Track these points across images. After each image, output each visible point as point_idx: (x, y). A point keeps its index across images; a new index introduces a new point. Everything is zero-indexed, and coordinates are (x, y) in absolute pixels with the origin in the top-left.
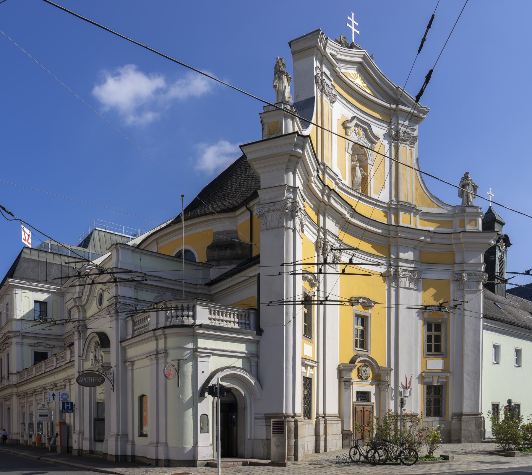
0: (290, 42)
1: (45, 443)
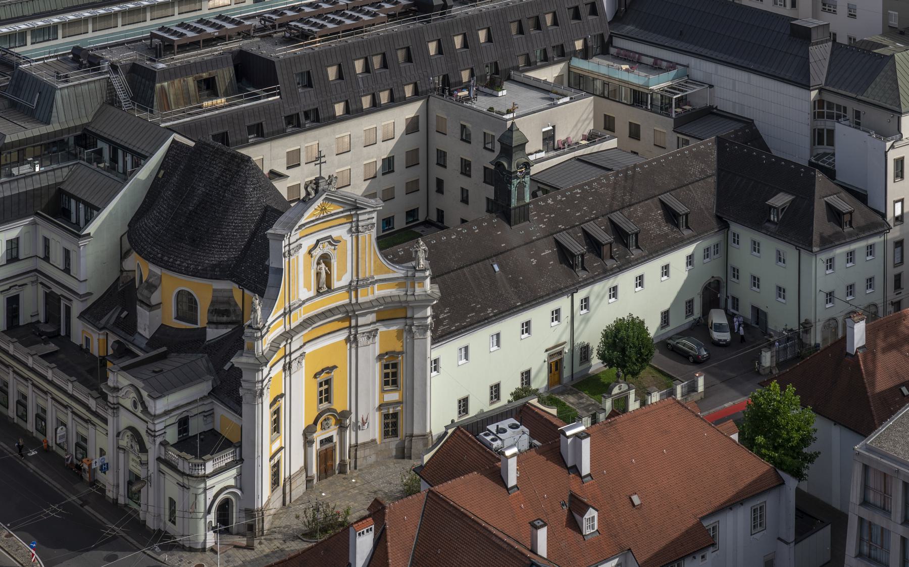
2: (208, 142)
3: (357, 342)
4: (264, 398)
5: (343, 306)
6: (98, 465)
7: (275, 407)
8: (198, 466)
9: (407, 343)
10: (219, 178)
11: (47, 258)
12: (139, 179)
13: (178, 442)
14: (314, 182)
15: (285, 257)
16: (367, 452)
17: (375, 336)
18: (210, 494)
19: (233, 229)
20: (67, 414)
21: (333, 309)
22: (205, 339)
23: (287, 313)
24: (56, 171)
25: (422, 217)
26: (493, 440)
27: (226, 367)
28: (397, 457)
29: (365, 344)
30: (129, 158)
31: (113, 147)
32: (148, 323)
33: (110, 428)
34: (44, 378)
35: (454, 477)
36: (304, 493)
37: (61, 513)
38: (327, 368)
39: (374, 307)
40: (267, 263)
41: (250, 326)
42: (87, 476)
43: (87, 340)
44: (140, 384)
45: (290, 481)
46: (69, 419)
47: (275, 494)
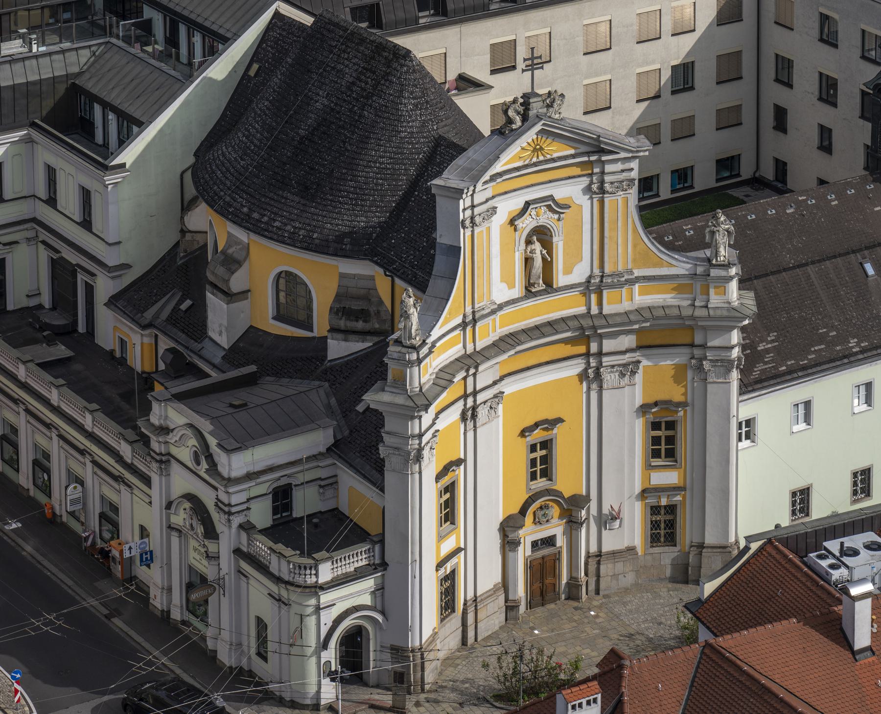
1: (61, 516)
2: (337, 20)
3: (601, 381)
4: (424, 463)
5: (576, 317)
6: (136, 552)
7: (446, 480)
8: (305, 568)
9: (693, 388)
10: (353, 83)
11: (52, 201)
12: (210, 79)
13: (272, 527)
14: (521, 100)
15: (464, 227)
16: (620, 567)
17: (633, 373)
18: (328, 618)
19: (377, 174)
20: (85, 464)
21: (556, 321)
22: (326, 357)
23: (469, 323)
24: (67, 54)
25: (746, 171)
26: (833, 566)
27: (360, 408)
28: (673, 580)
29: (616, 385)
30: (197, 39)
31: (171, 19)
32: (225, 323)
33: (155, 492)
34: (46, 402)
35: (755, 626)
36: (501, 628)
37: (59, 629)
38: (546, 421)
39: (631, 323)
40: (434, 236)
41: (398, 342)
42: (117, 570)
43: (123, 343)
44: (206, 426)
45: (476, 606)
46: (87, 472)
47: (448, 625)
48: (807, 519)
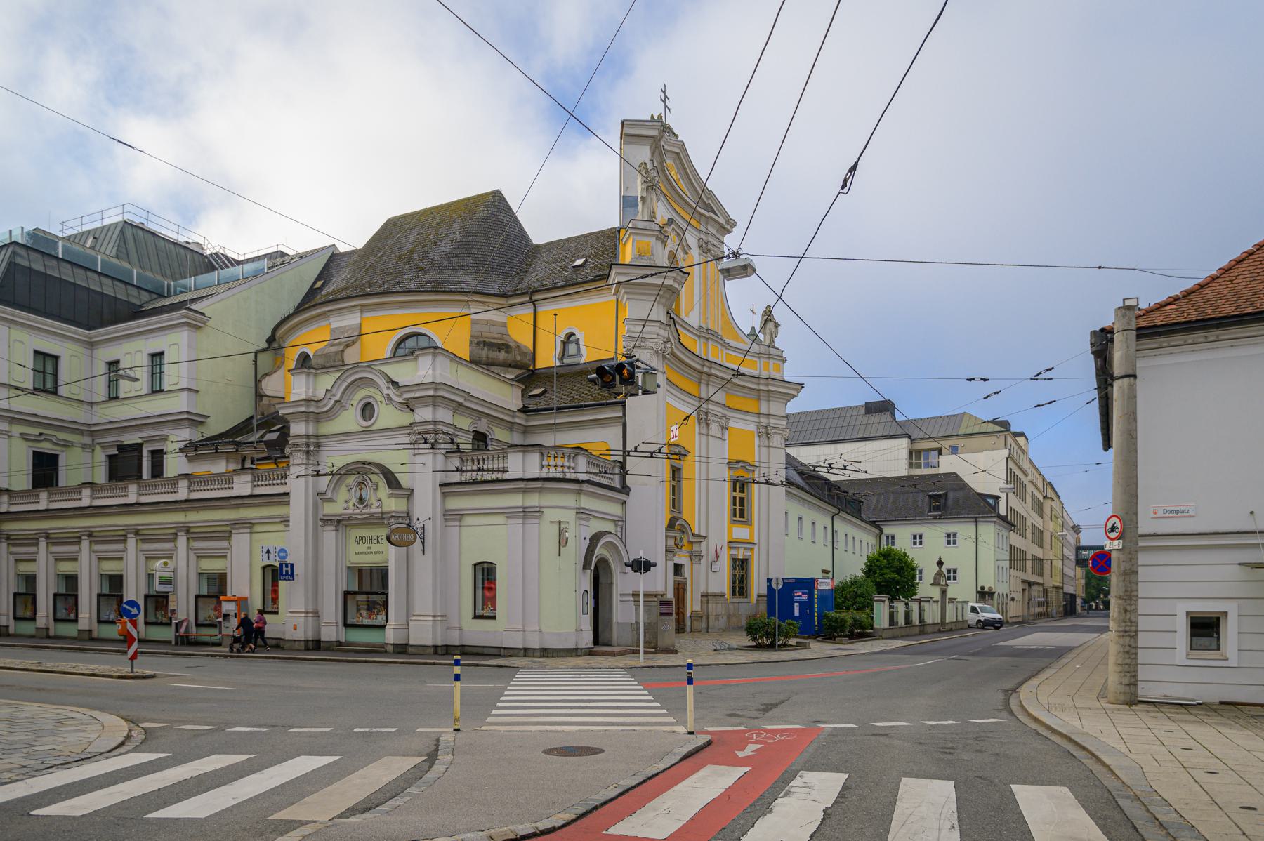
0: (624, 121)
48: (674, 603)
